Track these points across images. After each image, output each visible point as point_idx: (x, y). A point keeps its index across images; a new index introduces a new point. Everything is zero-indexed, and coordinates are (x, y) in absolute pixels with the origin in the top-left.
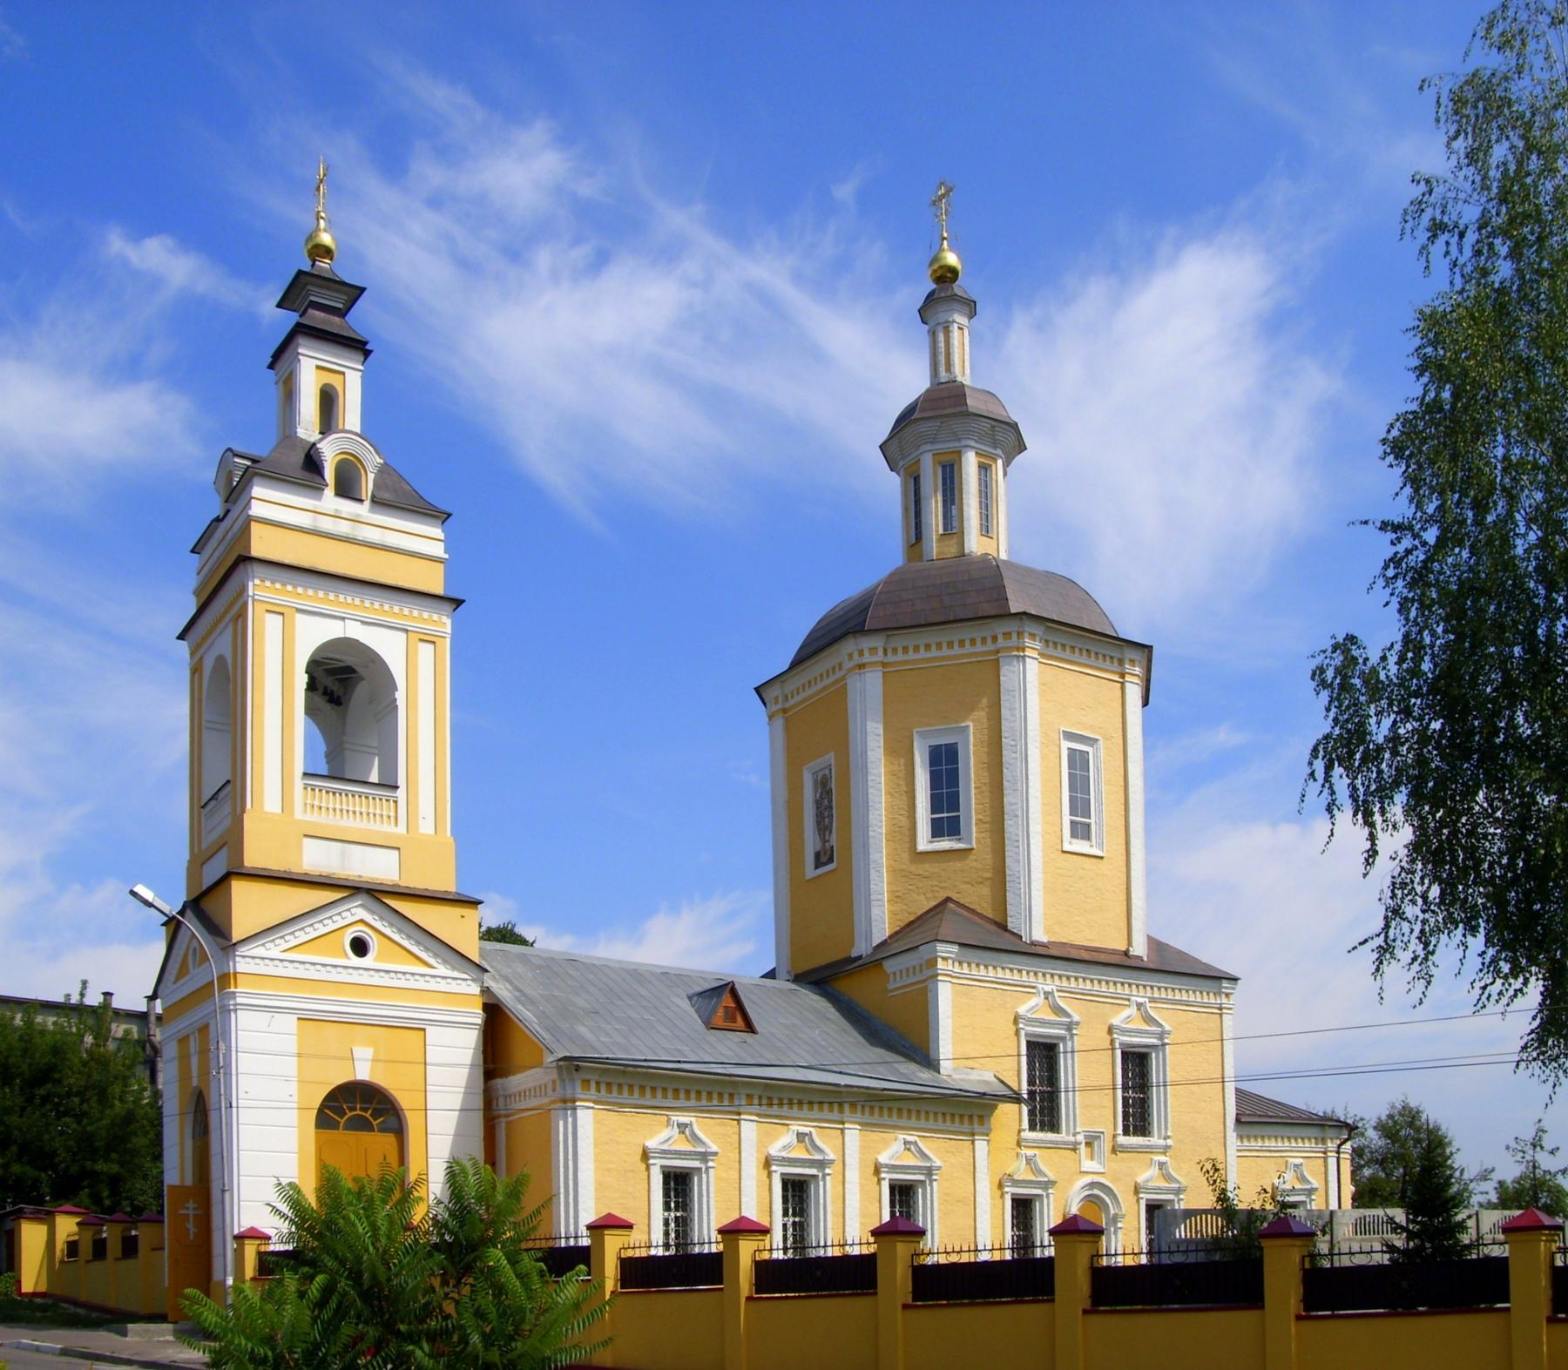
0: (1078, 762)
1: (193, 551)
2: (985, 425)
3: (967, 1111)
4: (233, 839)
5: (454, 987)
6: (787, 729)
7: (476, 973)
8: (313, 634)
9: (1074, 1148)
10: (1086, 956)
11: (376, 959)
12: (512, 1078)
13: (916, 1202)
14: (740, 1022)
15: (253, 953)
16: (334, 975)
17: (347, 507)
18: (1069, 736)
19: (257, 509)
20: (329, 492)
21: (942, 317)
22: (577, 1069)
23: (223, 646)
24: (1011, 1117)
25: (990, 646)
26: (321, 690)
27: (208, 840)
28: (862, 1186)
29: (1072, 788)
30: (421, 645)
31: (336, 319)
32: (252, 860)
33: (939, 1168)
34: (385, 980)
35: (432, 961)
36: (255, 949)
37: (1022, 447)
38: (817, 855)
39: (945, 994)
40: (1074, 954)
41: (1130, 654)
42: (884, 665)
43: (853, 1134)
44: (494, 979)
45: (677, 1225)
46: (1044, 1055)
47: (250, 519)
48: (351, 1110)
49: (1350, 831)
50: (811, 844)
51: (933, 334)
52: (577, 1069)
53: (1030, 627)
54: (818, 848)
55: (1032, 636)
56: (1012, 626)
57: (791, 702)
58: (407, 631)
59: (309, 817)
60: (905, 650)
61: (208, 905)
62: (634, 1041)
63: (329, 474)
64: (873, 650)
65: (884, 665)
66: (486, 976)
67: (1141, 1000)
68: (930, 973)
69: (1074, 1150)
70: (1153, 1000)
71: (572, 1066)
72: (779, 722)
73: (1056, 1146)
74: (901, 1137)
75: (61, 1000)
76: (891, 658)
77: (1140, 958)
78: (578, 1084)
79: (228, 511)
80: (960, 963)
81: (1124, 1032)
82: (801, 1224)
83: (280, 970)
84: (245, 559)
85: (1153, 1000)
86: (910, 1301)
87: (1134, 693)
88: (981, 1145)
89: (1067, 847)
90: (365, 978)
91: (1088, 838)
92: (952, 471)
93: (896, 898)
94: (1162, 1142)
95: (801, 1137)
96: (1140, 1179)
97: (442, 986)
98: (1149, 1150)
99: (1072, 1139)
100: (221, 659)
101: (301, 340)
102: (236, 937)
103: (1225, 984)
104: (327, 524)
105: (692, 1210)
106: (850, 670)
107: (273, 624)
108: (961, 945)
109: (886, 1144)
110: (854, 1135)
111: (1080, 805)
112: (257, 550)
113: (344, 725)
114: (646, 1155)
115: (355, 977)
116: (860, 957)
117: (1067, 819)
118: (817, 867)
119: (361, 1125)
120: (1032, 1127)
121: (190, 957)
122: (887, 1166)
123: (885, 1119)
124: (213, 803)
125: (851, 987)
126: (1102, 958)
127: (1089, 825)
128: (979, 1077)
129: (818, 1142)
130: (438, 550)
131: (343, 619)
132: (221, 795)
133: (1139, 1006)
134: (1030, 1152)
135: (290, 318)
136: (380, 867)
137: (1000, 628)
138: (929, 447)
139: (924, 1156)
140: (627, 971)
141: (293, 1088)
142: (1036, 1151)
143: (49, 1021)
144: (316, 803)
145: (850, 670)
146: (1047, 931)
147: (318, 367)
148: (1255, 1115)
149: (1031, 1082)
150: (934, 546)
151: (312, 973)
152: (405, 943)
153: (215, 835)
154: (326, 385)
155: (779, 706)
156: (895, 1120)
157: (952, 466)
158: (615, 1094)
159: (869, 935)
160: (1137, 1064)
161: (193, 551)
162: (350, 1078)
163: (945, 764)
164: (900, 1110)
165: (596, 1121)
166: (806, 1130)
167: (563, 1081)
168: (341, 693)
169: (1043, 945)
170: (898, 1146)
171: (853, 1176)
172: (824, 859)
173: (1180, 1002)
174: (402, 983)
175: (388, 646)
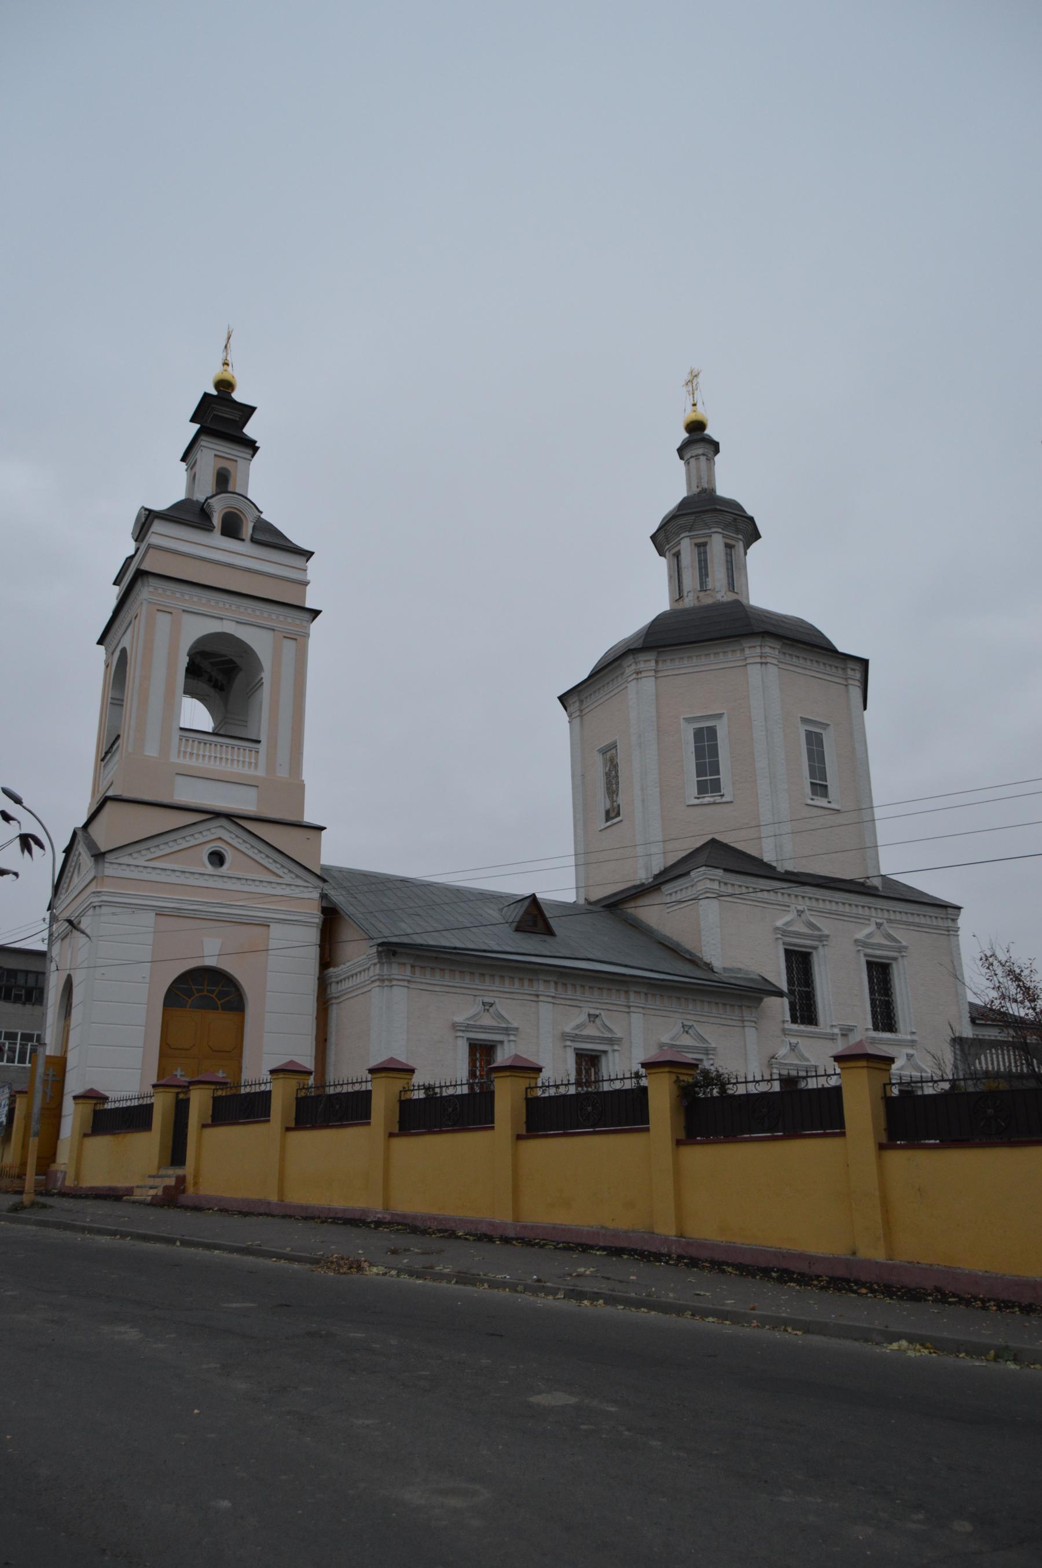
1: (115, 584)
2: (729, 518)
5: (297, 893)
18: (804, 720)
22: (394, 953)
24: (779, 1007)
29: (811, 758)
38: (607, 813)
41: (851, 665)
46: (800, 963)
48: (199, 991)
50: (602, 803)
54: (608, 806)
59: (181, 761)
63: (217, 520)
70: (889, 921)
77: (876, 888)
85: (889, 921)
86: (524, 1132)
87: (856, 693)
94: (909, 1037)
103: (950, 911)
108: (725, 870)
115: (211, 883)
117: (807, 781)
118: (607, 820)
120: (794, 1020)
127: (826, 786)
131: (222, 619)
133: (879, 925)
134: (794, 1041)
138: (687, 534)
139: (703, 1040)
142: (799, 1040)
144: (189, 750)
147: (216, 455)
160: (880, 975)
161: (115, 584)
166: (597, 1012)
172: (612, 815)
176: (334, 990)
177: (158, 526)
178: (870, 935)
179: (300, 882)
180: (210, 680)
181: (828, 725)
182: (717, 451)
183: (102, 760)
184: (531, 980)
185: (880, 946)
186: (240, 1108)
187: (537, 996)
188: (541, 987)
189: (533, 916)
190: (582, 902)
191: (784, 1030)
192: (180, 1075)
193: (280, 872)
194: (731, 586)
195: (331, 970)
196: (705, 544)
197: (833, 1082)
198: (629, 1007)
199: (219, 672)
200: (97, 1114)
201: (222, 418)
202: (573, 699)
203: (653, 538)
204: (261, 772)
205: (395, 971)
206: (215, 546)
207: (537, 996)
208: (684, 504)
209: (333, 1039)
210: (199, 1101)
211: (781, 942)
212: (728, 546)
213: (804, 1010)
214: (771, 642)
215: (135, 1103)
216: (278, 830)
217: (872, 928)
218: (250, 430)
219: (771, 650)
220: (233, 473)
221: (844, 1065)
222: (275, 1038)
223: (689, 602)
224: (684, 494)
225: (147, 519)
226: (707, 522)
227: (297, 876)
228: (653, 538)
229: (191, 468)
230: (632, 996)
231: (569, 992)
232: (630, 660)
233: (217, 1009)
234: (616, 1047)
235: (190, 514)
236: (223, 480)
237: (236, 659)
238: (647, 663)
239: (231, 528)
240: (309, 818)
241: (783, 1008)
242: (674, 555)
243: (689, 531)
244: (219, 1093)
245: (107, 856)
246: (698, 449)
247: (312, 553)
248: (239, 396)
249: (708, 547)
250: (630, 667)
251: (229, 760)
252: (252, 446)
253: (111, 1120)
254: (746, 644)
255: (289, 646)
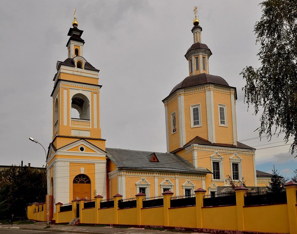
0: (222, 110)
2: (204, 50)
5: (100, 156)
8: (73, 93)
12: (111, 172)
14: (156, 160)
15: (61, 151)
17: (79, 70)
18: (192, 106)
22: (122, 169)
33: (195, 186)
36: (61, 150)
37: (211, 54)
38: (174, 130)
44: (109, 154)
46: (216, 165)
48: (80, 179)
49: (252, 106)
50: (172, 128)
51: (194, 34)
59: (72, 126)
63: (76, 64)
65: (184, 94)
77: (235, 146)
81: (232, 160)
86: (170, 208)
87: (233, 96)
89: (220, 125)
90: (83, 155)
91: (224, 123)
97: (98, 156)
100: (57, 99)
104: (75, 73)
107: (65, 92)
108: (199, 144)
109: (184, 182)
111: (222, 117)
113: (82, 110)
115: (81, 155)
116: (181, 148)
117: (220, 120)
119: (82, 182)
120: (214, 178)
122: (184, 186)
127: (224, 121)
134: (214, 183)
136: (87, 135)
140: (136, 152)
143: (39, 170)
144: (74, 123)
146: (216, 141)
148: (261, 175)
149: (214, 169)
154: (76, 49)
159: (182, 144)
160: (235, 166)
162: (80, 174)
170: (186, 182)
171: (177, 188)
175: (88, 94)
176: (110, 178)
177: (62, 67)
178: (233, 157)
179: (101, 153)
181: (225, 105)
182: (201, 30)
183: (55, 126)
184: (153, 173)
185: (236, 160)
186: (90, 205)
187: (154, 177)
188: (155, 175)
189: (154, 157)
190: (168, 153)
191: (212, 181)
192: (78, 199)
193: (96, 151)
194: (204, 69)
195: (109, 173)
196: (198, 57)
197: (162, 198)
198: (175, 178)
199: (79, 102)
200: (61, 208)
201: (75, 34)
202: (166, 101)
203: (185, 56)
204: (91, 128)
205: (122, 173)
206: (75, 70)
207: (154, 177)
208: (193, 46)
209: (110, 189)
210: (82, 204)
211: (212, 160)
212: (203, 58)
213: (217, 175)
214: (211, 85)
215: (69, 205)
216: (95, 140)
217: (234, 155)
218: (82, 37)
219: (212, 87)
220: (79, 49)
221: (196, 193)
222: (99, 188)
223: (195, 73)
225: (60, 65)
226: (198, 50)
227: (100, 152)
228: (185, 56)
229: (69, 48)
230: (176, 175)
231: (162, 175)
232: (178, 91)
233: (85, 183)
234: (172, 187)
235: (69, 62)
236: (77, 52)
237: (84, 100)
238: (182, 92)
239: (79, 66)
240: (102, 138)
241: (231, 170)
242: (190, 60)
244: (85, 202)
245: (58, 150)
246: (198, 30)
247: (99, 70)
248: (79, 28)
249: (198, 58)
250: (178, 92)
251: (82, 125)
252: (83, 42)
253: (65, 209)
254: (205, 86)
255: (95, 95)
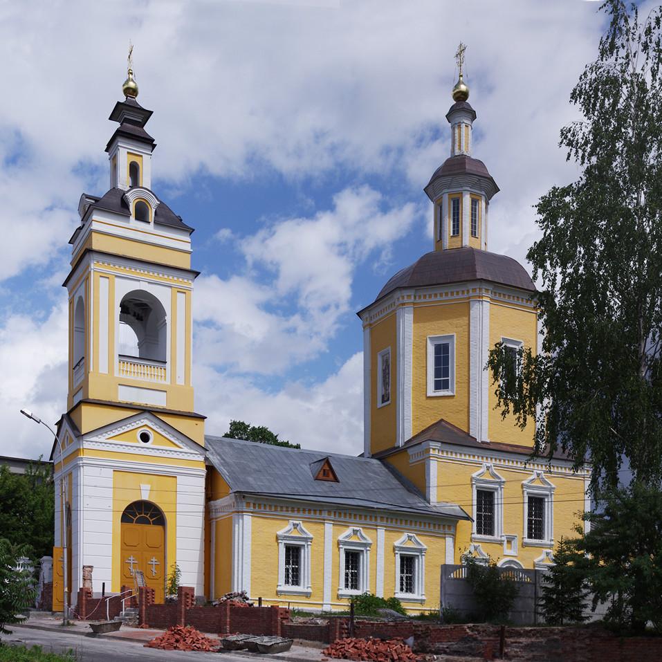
3: (445, 523)
4: (84, 386)
6: (371, 334)
7: (202, 451)
8: (124, 288)
9: (501, 543)
10: (510, 449)
11: (152, 444)
12: (218, 501)
13: (414, 566)
14: (331, 476)
15: (92, 439)
16: (132, 451)
17: (141, 225)
19: (95, 226)
20: (132, 218)
21: (457, 120)
23: (81, 292)
24: (468, 529)
25: (466, 295)
26: (132, 313)
27: (76, 385)
28: (386, 557)
30: (179, 294)
31: (139, 129)
32: (93, 395)
33: (426, 549)
34: (158, 454)
35: (181, 445)
38: (383, 396)
39: (434, 467)
40: (504, 448)
42: (414, 304)
43: (381, 532)
44: (212, 454)
45: (352, 576)
46: (486, 499)
47: (92, 231)
52: (244, 497)
53: (485, 286)
55: (487, 290)
56: (477, 286)
57: (374, 320)
58: (171, 287)
60: (425, 296)
61: (73, 416)
62: (275, 485)
64: (409, 296)
65: (414, 304)
66: (207, 452)
67: (539, 472)
68: (427, 456)
69: (501, 544)
71: (241, 495)
72: (368, 331)
73: (491, 542)
74: (406, 534)
75: (36, 458)
76: (418, 301)
78: (244, 504)
79: (84, 225)
80: (442, 451)
81: (529, 487)
82: (410, 577)
83: (105, 448)
84: (89, 251)
88: (449, 540)
90: (147, 452)
92: (458, 204)
93: (416, 418)
95: (295, 526)
96: (536, 560)
97: (186, 457)
98: (542, 546)
99: (499, 538)
100: (80, 298)
101: (119, 139)
102: (83, 432)
105: (300, 565)
106: (398, 306)
107: (104, 283)
108: (442, 443)
110: (329, 527)
112: (95, 247)
114: (277, 538)
118: (383, 403)
119: (143, 521)
121: (66, 440)
123: (398, 525)
124: (78, 367)
125: (395, 461)
126: (520, 450)
128: (452, 508)
129: (363, 534)
130: (188, 247)
131: (139, 281)
132: (81, 363)
134: (476, 544)
135: (117, 125)
137: (470, 286)
138: (446, 191)
141: (110, 503)
142: (480, 544)
144: (132, 370)
145: (398, 306)
146: (490, 436)
150: (448, 243)
151: (121, 449)
152: (168, 436)
153: (77, 384)
155: (368, 323)
156: (403, 525)
157: (458, 200)
158: (368, 520)
162: (139, 499)
163: (442, 353)
164: (355, 515)
165: (253, 522)
166: (358, 529)
167: (237, 502)
168: (143, 315)
169: (487, 443)
171: (381, 552)
172: (386, 399)
173: (560, 473)
174: (166, 455)
175: (162, 294)
180: (134, 315)
195: (212, 502)
204: (168, 382)
218: (150, 128)
224: (449, 157)
232: (398, 294)
243: (471, 188)
